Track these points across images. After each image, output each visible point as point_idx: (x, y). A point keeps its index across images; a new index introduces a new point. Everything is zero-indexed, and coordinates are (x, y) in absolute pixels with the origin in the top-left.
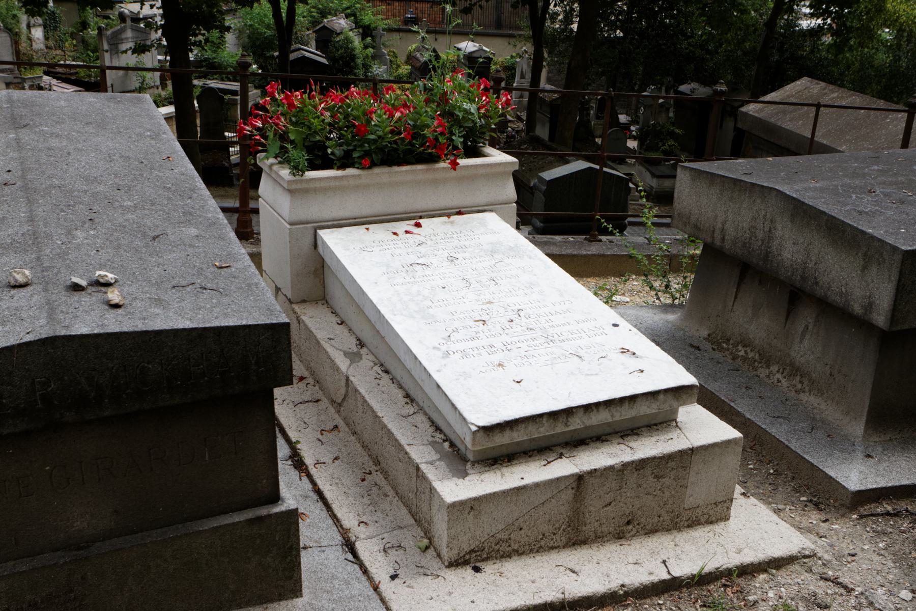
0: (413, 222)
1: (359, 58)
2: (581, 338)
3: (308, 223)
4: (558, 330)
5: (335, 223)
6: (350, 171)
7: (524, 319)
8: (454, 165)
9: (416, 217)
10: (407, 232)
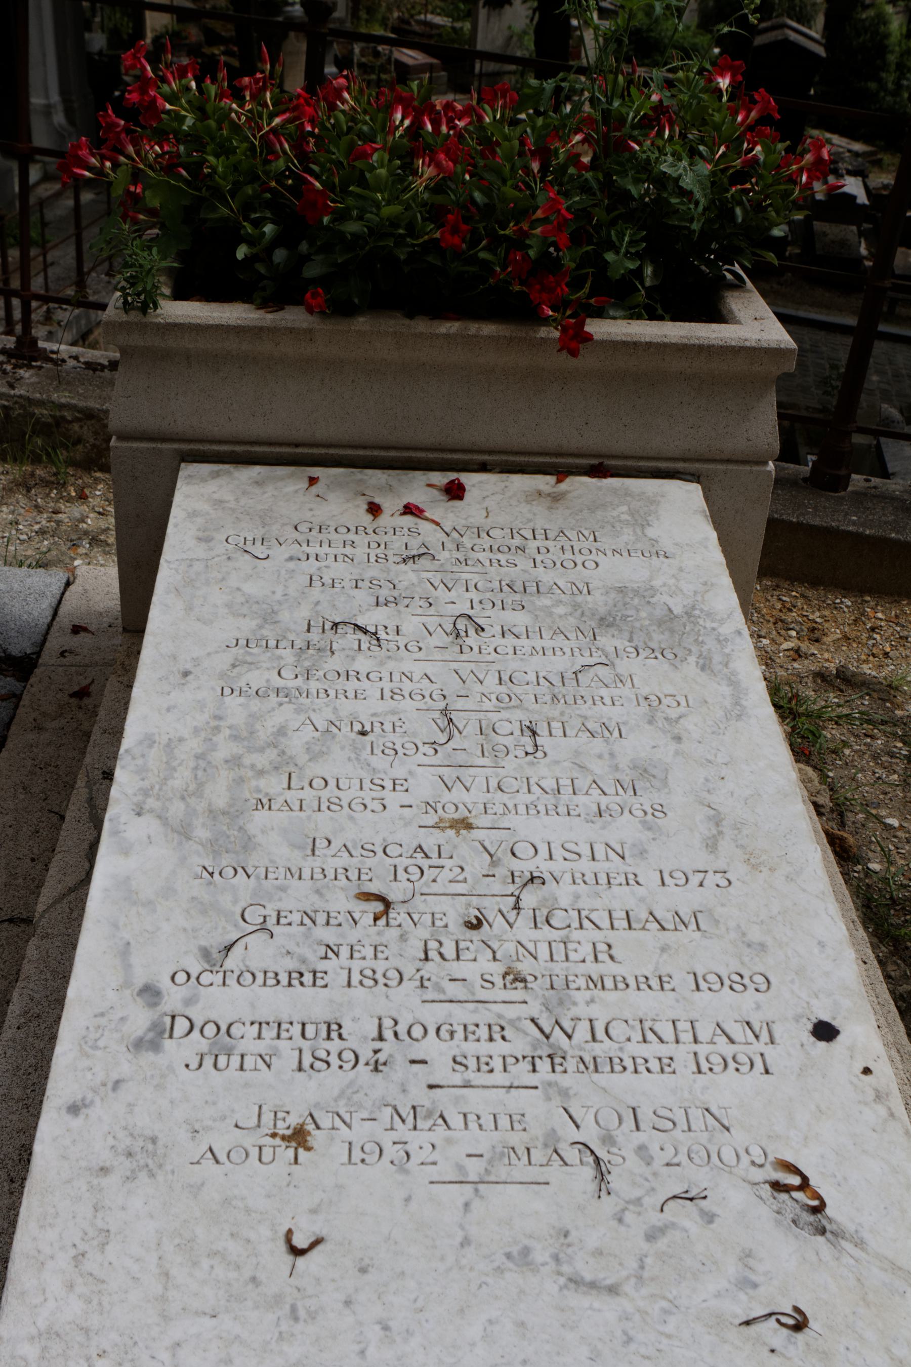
0: (441, 478)
1: (892, 52)
2: (666, 1065)
3: (164, 440)
4: (605, 1006)
5: (239, 449)
6: (294, 317)
7: (523, 923)
8: (575, 340)
9: (453, 463)
10: (410, 510)
